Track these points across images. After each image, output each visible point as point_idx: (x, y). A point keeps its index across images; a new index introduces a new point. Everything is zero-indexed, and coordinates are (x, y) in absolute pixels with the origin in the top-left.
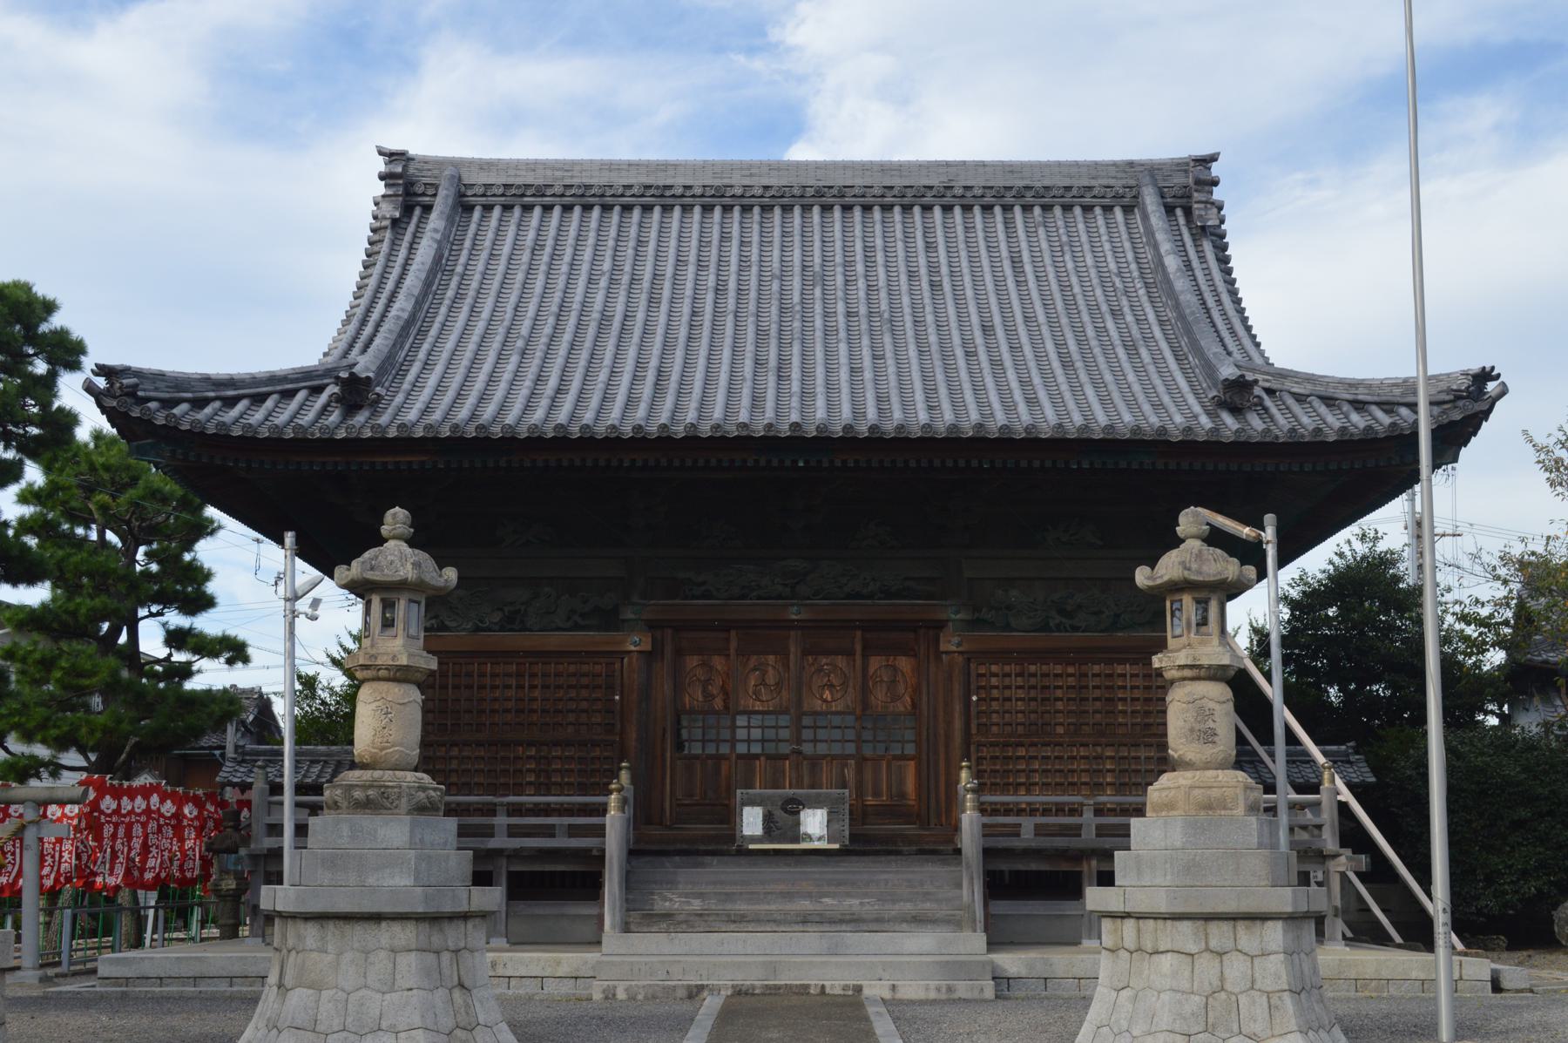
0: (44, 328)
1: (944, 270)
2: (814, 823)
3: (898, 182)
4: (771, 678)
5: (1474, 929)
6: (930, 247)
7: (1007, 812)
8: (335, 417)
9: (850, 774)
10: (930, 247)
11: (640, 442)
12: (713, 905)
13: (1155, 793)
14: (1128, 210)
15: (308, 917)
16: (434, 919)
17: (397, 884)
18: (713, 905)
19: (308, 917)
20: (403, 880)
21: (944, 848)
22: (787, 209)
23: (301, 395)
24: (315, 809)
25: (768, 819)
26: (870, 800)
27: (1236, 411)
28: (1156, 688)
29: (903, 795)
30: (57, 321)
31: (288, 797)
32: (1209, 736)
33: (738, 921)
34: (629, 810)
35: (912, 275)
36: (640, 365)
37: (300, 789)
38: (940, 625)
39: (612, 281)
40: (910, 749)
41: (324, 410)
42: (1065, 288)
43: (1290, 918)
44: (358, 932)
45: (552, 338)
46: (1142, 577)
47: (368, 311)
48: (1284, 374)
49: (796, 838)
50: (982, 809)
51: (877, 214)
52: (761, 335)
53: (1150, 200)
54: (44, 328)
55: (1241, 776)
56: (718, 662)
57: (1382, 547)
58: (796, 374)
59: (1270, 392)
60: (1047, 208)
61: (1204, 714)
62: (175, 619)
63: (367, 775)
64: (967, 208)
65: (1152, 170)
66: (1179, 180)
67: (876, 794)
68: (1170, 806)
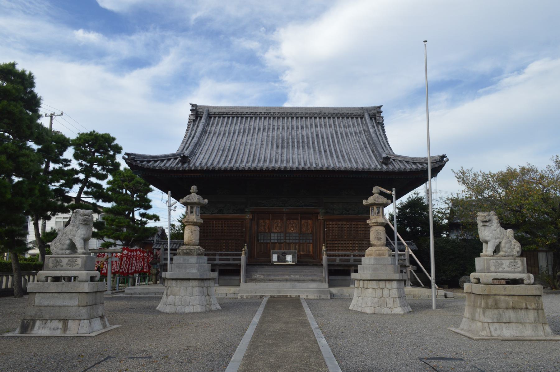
0: (113, 144)
1: (319, 132)
2: (289, 258)
3: (309, 112)
4: (279, 225)
6: (316, 126)
7: (333, 256)
8: (180, 165)
9: (297, 247)
10: (316, 126)
14: (361, 118)
15: (173, 279)
16: (202, 280)
17: (194, 272)
18: (266, 277)
19: (173, 279)
22: (283, 118)
23: (172, 160)
24: (175, 254)
25: (278, 257)
26: (302, 253)
28: (368, 227)
29: (309, 252)
30: (116, 142)
31: (169, 252)
32: (380, 239)
33: (271, 280)
34: (247, 255)
35: (312, 133)
36: (250, 153)
37: (171, 250)
38: (318, 213)
39: (243, 134)
40: (311, 241)
41: (177, 163)
42: (347, 136)
43: (398, 281)
44: (185, 283)
45: (230, 147)
46: (364, 202)
48: (397, 156)
50: (327, 255)
51: (304, 119)
53: (367, 116)
54: (113, 144)
55: (387, 248)
56: (267, 221)
57: (419, 196)
58: (285, 155)
59: (394, 160)
60: (343, 118)
61: (378, 234)
62: (142, 211)
63: (187, 247)
64: (325, 118)
65: (367, 109)
66: (373, 111)
67: (303, 252)
68: (371, 255)
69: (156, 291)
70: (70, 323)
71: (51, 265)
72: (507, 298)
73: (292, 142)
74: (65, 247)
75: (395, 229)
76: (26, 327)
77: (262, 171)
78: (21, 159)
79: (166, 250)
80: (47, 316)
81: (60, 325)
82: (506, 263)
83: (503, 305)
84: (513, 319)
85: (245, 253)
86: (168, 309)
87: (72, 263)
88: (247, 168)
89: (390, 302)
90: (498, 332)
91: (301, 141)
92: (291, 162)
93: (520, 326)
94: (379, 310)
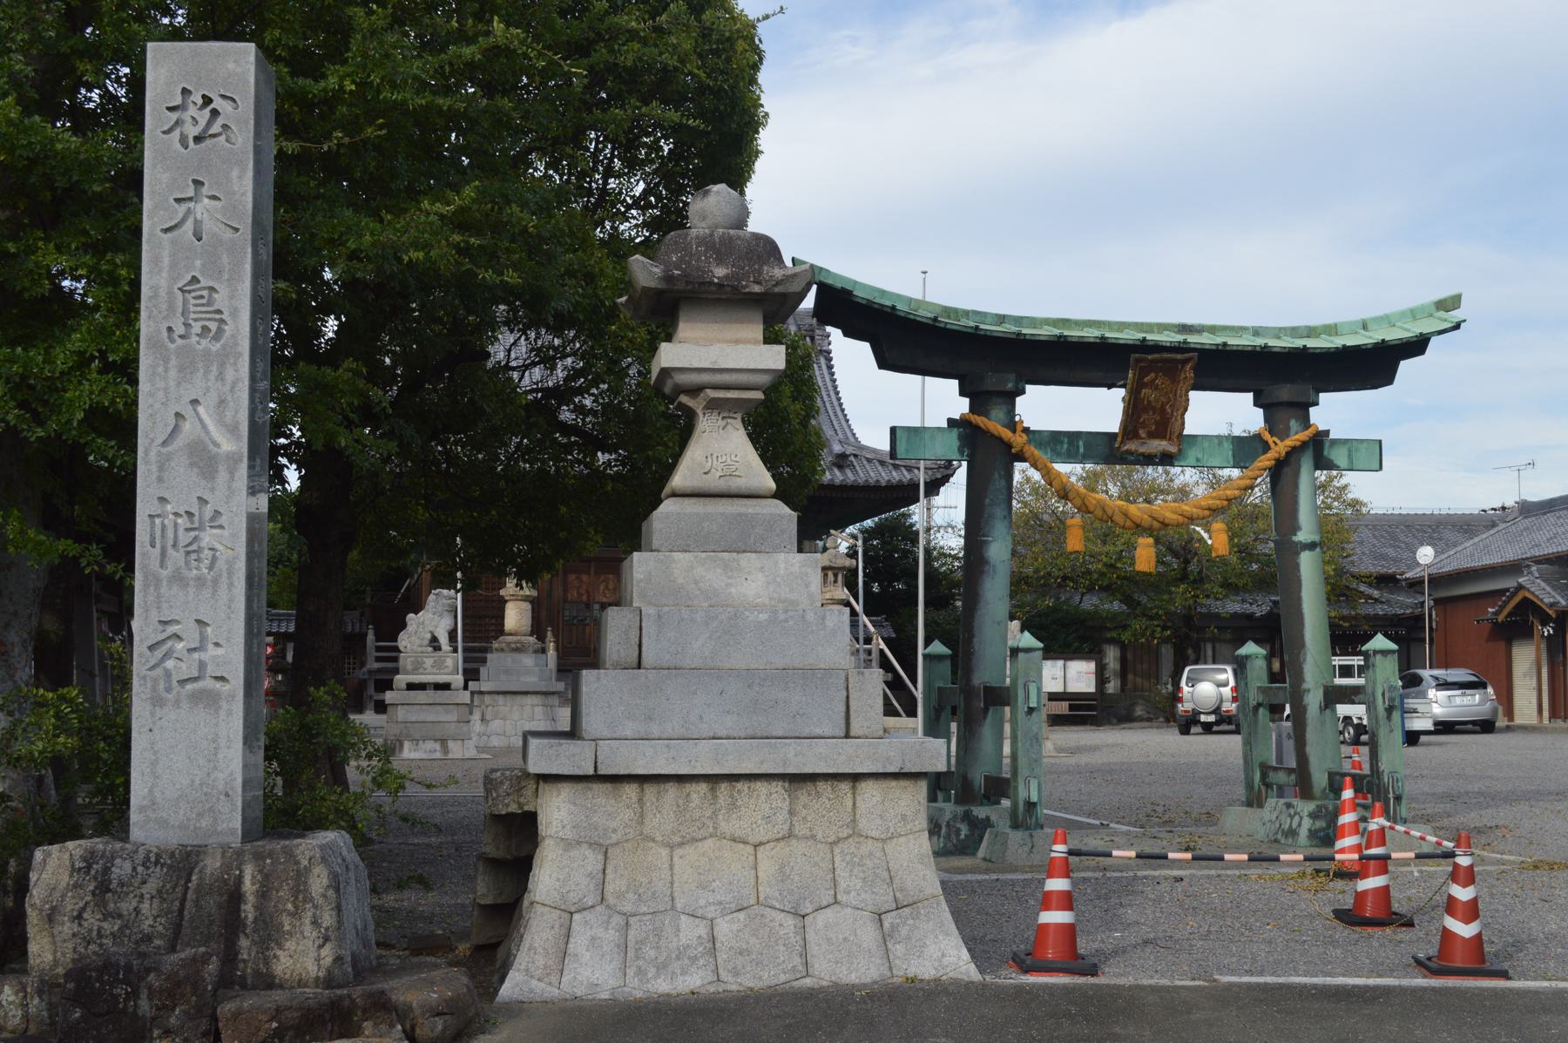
5: (956, 803)
15: (498, 693)
16: (546, 694)
17: (531, 681)
19: (498, 693)
20: (535, 679)
27: (840, 467)
44: (519, 699)
48: (864, 448)
56: (585, 578)
59: (856, 456)
63: (515, 638)
70: (451, 744)
74: (426, 642)
75: (859, 608)
80: (417, 736)
81: (437, 746)
87: (439, 665)
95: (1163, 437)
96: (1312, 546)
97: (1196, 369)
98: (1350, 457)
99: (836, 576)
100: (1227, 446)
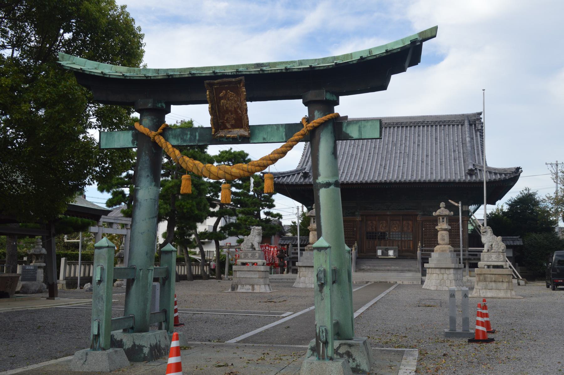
0: (246, 159)
1: (421, 142)
2: (391, 253)
3: (413, 121)
4: (384, 225)
6: (419, 135)
7: (428, 251)
8: (302, 180)
9: (400, 243)
10: (419, 135)
11: (357, 184)
12: (372, 268)
13: (435, 249)
14: (462, 125)
15: (304, 267)
18: (372, 268)
19: (304, 267)
21: (414, 258)
22: (390, 127)
23: (296, 175)
24: (304, 250)
25: (382, 252)
26: (404, 249)
27: (471, 175)
28: (437, 231)
29: (410, 248)
30: (249, 157)
31: (299, 248)
32: (444, 240)
33: (376, 270)
34: (357, 250)
35: (414, 143)
36: (358, 166)
37: (301, 246)
38: (417, 215)
39: (354, 146)
40: (411, 239)
41: (300, 178)
42: (445, 145)
43: (454, 268)
45: (342, 160)
46: (434, 214)
47: (307, 154)
49: (388, 256)
50: (422, 251)
51: (409, 128)
52: (382, 158)
53: (466, 123)
54: (246, 159)
55: (450, 246)
56: (374, 222)
57: (530, 192)
58: (387, 168)
60: (445, 125)
61: (443, 236)
62: (266, 210)
64: (428, 126)
65: (468, 116)
66: (474, 118)
67: (405, 247)
68: (437, 251)
69: (288, 278)
70: (255, 286)
71: (243, 257)
72: (492, 276)
73: (396, 153)
74: (249, 247)
76: (234, 288)
77: (366, 183)
78: (202, 187)
79: (296, 246)
80: (243, 283)
81: (250, 287)
82: (494, 256)
83: (489, 279)
84: (494, 287)
85: (355, 249)
86: (301, 286)
87: (253, 256)
88: (354, 182)
89: (448, 282)
90: (484, 294)
91: (403, 152)
92: (391, 175)
93: (498, 291)
94: (440, 288)
95: (241, 127)
96: (327, 185)
97: (246, 86)
98: (360, 131)
99: (443, 218)
100: (282, 130)
